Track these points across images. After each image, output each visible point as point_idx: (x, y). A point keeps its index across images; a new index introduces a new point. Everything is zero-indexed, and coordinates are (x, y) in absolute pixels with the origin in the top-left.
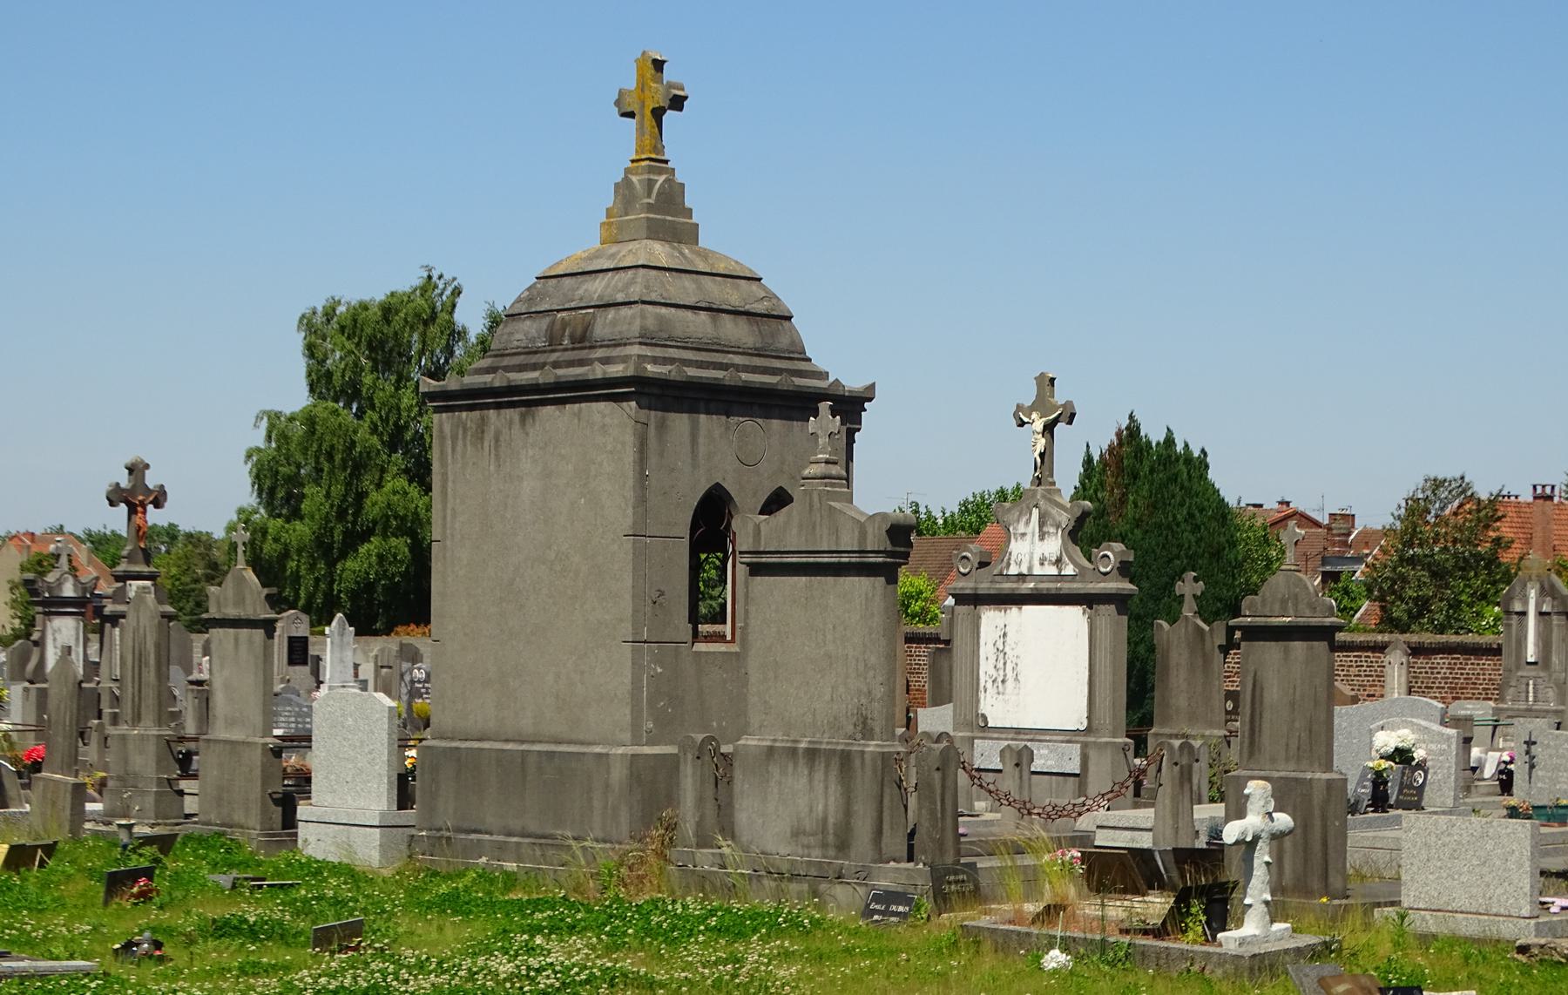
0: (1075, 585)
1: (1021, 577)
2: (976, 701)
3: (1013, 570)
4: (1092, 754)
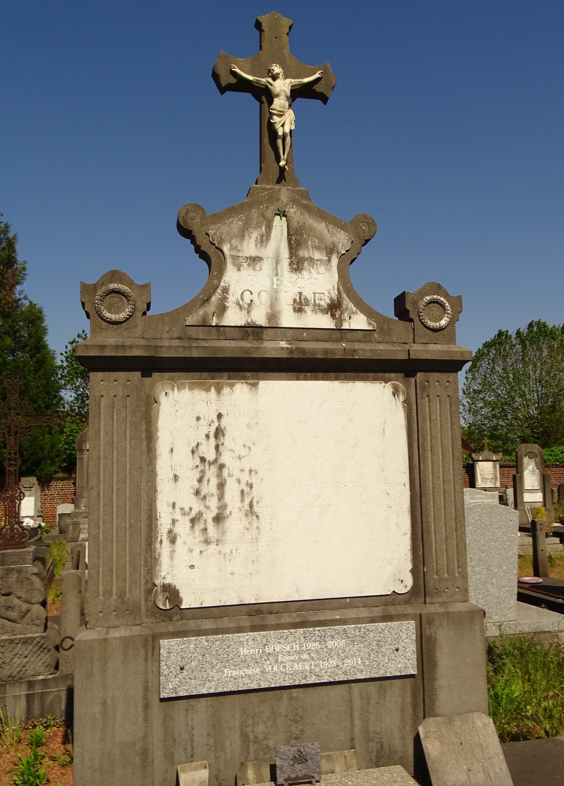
0: (381, 347)
1: (252, 331)
2: (151, 561)
3: (234, 318)
4: (444, 636)
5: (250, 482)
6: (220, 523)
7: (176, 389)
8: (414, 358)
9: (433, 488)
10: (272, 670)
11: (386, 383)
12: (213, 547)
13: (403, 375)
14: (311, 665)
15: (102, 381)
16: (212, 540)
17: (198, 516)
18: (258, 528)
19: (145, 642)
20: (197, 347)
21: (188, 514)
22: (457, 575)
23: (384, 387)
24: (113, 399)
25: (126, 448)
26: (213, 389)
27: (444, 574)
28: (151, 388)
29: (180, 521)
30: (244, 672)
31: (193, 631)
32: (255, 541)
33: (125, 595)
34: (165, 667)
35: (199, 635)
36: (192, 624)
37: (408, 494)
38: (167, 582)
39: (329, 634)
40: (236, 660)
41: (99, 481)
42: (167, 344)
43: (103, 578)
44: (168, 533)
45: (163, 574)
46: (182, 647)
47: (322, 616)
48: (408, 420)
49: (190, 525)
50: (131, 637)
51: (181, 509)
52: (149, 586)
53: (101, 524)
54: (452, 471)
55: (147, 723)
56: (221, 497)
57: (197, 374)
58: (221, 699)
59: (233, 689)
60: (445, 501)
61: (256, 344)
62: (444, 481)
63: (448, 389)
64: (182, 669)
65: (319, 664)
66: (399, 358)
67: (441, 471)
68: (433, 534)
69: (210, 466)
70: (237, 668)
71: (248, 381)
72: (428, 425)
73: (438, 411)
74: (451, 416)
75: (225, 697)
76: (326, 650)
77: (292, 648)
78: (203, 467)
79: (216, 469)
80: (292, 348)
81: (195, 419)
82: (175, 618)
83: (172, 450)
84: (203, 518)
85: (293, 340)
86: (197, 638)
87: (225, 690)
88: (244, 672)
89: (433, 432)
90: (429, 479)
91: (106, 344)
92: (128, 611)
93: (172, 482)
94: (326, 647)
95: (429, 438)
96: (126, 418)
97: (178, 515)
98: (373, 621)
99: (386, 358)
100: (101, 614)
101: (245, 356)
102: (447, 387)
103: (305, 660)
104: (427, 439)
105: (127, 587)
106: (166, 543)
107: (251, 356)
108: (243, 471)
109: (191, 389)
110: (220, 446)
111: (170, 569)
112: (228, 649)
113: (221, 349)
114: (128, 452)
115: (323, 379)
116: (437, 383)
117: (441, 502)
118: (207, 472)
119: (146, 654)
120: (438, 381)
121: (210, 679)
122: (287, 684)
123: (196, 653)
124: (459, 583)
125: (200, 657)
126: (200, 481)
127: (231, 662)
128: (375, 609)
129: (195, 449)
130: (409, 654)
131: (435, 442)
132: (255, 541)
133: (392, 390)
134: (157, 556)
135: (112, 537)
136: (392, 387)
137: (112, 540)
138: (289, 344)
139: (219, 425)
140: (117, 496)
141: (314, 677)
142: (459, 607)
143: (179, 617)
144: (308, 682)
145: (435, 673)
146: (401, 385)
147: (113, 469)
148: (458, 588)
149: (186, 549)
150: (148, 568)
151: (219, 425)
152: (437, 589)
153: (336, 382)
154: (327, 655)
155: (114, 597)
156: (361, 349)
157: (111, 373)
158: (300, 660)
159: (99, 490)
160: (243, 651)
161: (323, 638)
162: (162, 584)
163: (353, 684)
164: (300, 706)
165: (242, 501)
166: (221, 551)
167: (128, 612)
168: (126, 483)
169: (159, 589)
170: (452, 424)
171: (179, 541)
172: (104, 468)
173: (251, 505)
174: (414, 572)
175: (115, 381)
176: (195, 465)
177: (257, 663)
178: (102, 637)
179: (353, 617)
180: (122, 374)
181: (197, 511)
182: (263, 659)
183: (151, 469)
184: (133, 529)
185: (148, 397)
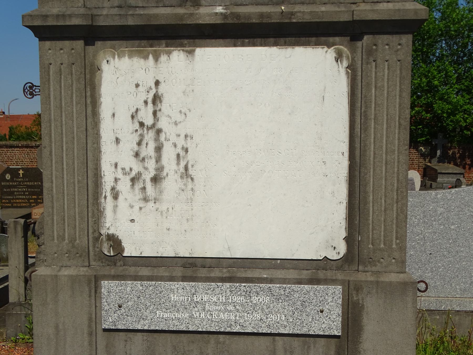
0: (323, 9)
2: (97, 214)
4: (372, 306)
5: (185, 146)
6: (157, 183)
7: (116, 57)
8: (358, 19)
9: (374, 158)
10: (200, 316)
11: (329, 47)
12: (151, 204)
13: (349, 38)
14: (236, 316)
15: (50, 49)
16: (150, 198)
17: (138, 176)
18: (192, 189)
19: (89, 282)
20: (132, 15)
21: (129, 174)
22: (394, 246)
23: (326, 52)
24: (60, 67)
25: (73, 112)
26: (151, 57)
27: (380, 245)
28: (95, 56)
29: (122, 180)
30: (174, 315)
31: (130, 276)
32: (190, 201)
33: (75, 240)
34: (106, 304)
35: (135, 280)
36: (132, 270)
37: (346, 163)
38: (111, 232)
39: (254, 290)
40: (167, 304)
41: (51, 141)
42: (105, 12)
43: (57, 225)
44: (111, 190)
45: (107, 225)
46: (120, 288)
47: (249, 274)
48: (351, 87)
49: (131, 183)
50: (77, 276)
51: (123, 169)
52: (96, 235)
53: (54, 179)
54: (397, 142)
55: (91, 347)
56: (158, 159)
57: (137, 42)
58: (156, 335)
59: (164, 329)
60: (386, 172)
61: (192, 10)
62: (386, 151)
63: (399, 52)
64: (120, 307)
65: (244, 316)
66: (341, 20)
67: (384, 141)
68: (371, 204)
69: (148, 130)
70: (168, 311)
71: (185, 49)
72: (373, 91)
73: (386, 77)
74: (400, 82)
75: (158, 334)
76: (250, 304)
77: (219, 299)
78: (142, 131)
79: (153, 134)
80: (226, 13)
81: (135, 86)
82: (119, 264)
83: (114, 115)
84: (142, 178)
85: (231, 4)
86: (133, 282)
87: (157, 328)
88: (174, 315)
89: (377, 99)
90: (370, 148)
91: (48, 14)
92: (83, 255)
93: (114, 145)
94: (251, 302)
95: (373, 106)
96: (72, 84)
97: (120, 175)
98: (300, 283)
99: (326, 20)
100: (56, 255)
101: (179, 22)
102: (398, 50)
103: (231, 311)
104: (371, 107)
105: (77, 234)
106: (109, 198)
107: (184, 22)
108: (179, 136)
109: (130, 57)
110: (158, 112)
111: (113, 221)
112: (160, 295)
113: (156, 16)
114: (75, 116)
115: (261, 45)
116: (387, 47)
117: (382, 172)
118: (146, 136)
119: (90, 292)
120: (387, 45)
121: (144, 317)
122: (213, 329)
123: (132, 295)
124: (396, 255)
125: (136, 299)
126: (139, 144)
127: (163, 305)
128: (305, 272)
129: (134, 114)
130: (334, 317)
131: (379, 111)
132: (190, 201)
133: (334, 55)
134: (102, 210)
135: (63, 190)
136: (335, 52)
137: (63, 193)
138: (225, 9)
139: (157, 92)
140: (67, 155)
141: (238, 327)
142: (393, 277)
143: (122, 263)
144: (232, 331)
145: (360, 337)
146: (346, 49)
147: (62, 131)
148: (394, 259)
149: (127, 204)
150: (95, 219)
151: (157, 92)
152: (371, 258)
153: (275, 48)
154: (251, 309)
155: (67, 241)
156: (300, 12)
157: (57, 42)
158: (226, 310)
159: (51, 149)
160: (174, 297)
161: (248, 293)
162: (106, 234)
163: (277, 338)
164: (226, 350)
165: (178, 164)
166: (158, 208)
167: (78, 255)
168: (73, 143)
169: (104, 238)
170: (400, 91)
171: (121, 198)
172: (55, 130)
173: (186, 168)
174: (349, 240)
175: (61, 49)
176: (135, 129)
177: (186, 309)
178: (53, 274)
179: (280, 277)
180: (67, 43)
181: (137, 172)
182: (192, 306)
183: (96, 132)
184: (81, 185)
185: (92, 65)
